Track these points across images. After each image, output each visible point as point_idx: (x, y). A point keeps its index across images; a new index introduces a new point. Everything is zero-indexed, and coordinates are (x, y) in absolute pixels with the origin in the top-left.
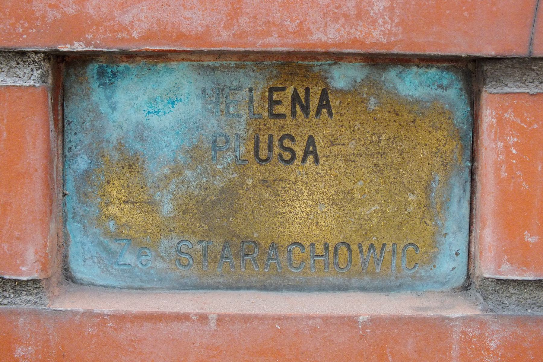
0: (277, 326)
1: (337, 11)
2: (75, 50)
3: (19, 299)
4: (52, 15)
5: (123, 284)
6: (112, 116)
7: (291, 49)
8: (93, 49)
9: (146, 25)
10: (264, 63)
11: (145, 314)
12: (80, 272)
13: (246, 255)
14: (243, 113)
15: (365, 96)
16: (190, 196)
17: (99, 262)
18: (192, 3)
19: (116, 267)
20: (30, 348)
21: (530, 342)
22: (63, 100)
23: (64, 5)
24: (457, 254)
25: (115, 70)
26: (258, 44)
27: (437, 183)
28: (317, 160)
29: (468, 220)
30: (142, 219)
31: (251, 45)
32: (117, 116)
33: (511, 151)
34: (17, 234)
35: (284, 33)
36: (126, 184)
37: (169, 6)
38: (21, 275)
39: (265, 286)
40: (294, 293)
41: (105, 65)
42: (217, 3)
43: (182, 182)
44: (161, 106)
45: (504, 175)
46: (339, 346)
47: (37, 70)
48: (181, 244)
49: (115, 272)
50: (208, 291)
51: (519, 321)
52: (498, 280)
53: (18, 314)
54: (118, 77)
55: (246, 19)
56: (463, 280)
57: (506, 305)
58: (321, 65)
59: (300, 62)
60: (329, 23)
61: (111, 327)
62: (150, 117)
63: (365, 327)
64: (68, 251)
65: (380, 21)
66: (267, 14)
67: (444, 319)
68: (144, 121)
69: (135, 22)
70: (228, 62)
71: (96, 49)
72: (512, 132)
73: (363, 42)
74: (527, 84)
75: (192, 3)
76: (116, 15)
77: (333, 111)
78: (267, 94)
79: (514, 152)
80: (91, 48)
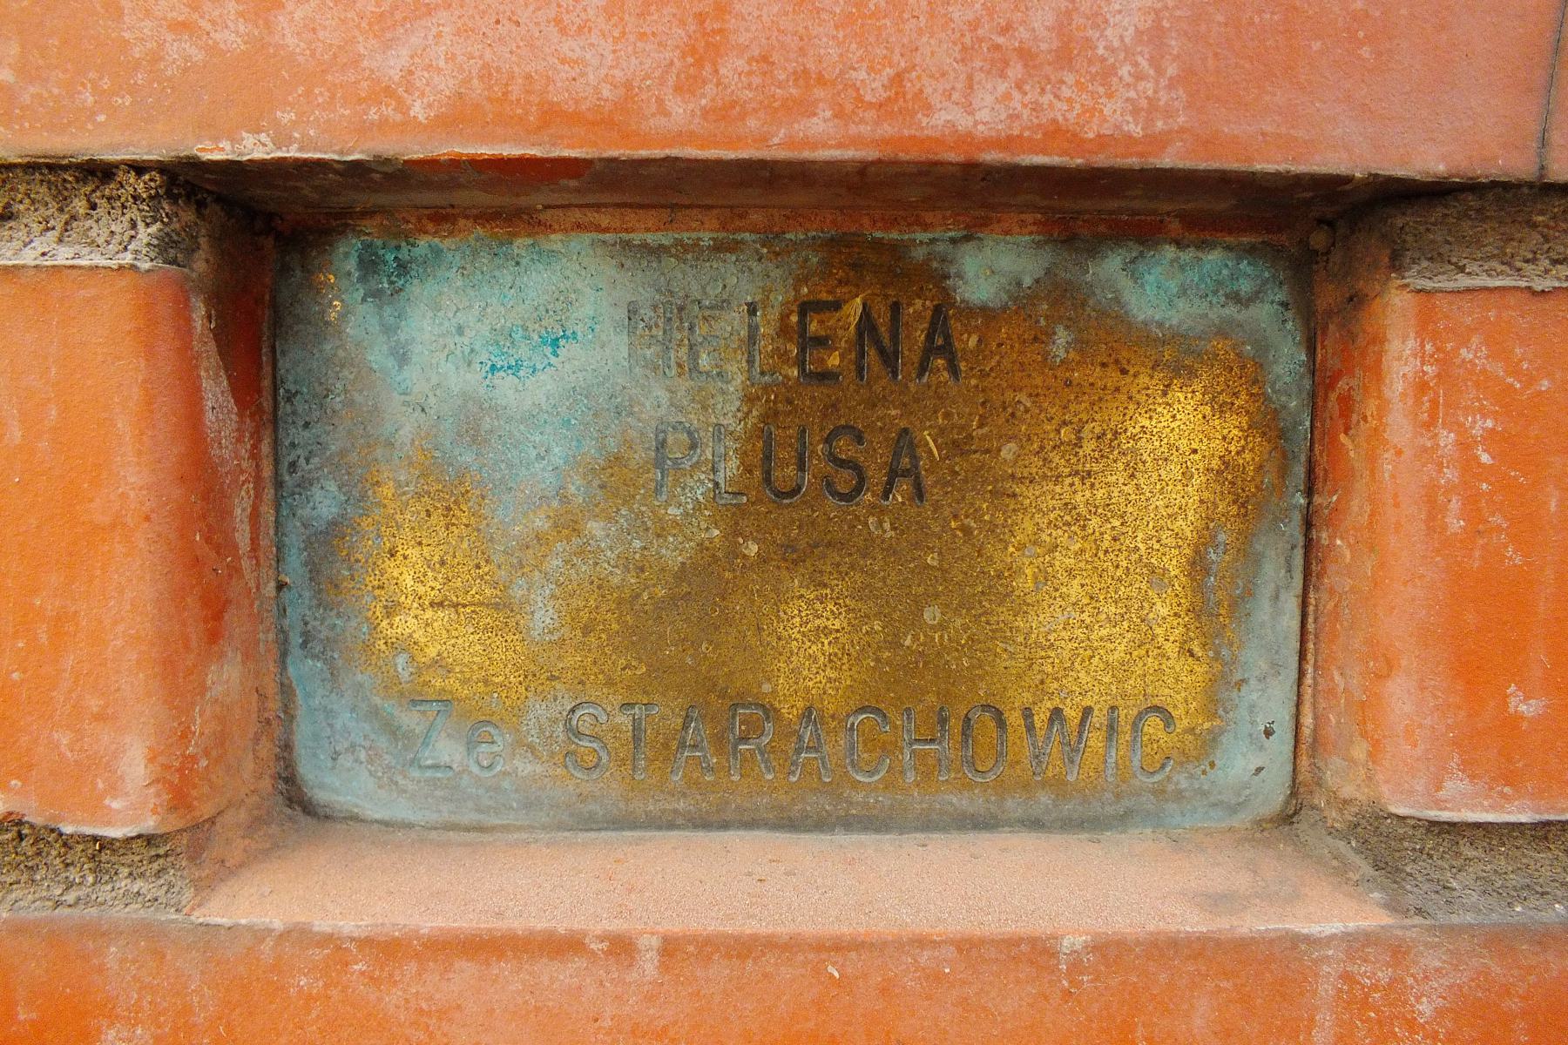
0: (831, 969)
1: (1000, 40)
2: (245, 158)
3: (109, 887)
4: (179, 50)
5: (433, 817)
6: (398, 379)
7: (871, 154)
8: (298, 155)
9: (451, 82)
10: (788, 236)
11: (457, 937)
12: (322, 786)
13: (744, 739)
14: (735, 369)
15: (1043, 322)
16: (599, 587)
17: (370, 761)
18: (583, 16)
19: (416, 774)
20: (139, 1032)
21: (1523, 998)
22: (275, 336)
23: (214, 23)
24: (1268, 733)
25: (404, 254)
26: (776, 140)
27: (1220, 551)
28: (919, 493)
29: (1295, 644)
30: (478, 647)
31: (755, 141)
32: (411, 375)
33: (1477, 458)
34: (94, 703)
35: (849, 107)
36: (436, 558)
37: (518, 24)
38: (109, 824)
39: (790, 818)
40: (863, 837)
41: (379, 243)
42: (655, 17)
43: (580, 552)
44: (523, 351)
45: (1456, 524)
46: (1004, 1022)
47: (148, 225)
48: (579, 713)
49: (411, 787)
50: (649, 834)
51: (1499, 940)
52: (1433, 823)
53: (101, 933)
54: (413, 273)
55: (741, 63)
56: (1281, 798)
57: (1455, 894)
58: (933, 241)
59: (878, 234)
60: (978, 76)
61: (363, 973)
62: (496, 381)
63: (1076, 967)
64: (291, 732)
65: (1125, 71)
66: (801, 49)
67: (1295, 941)
68: (482, 391)
69: (418, 73)
70: (694, 235)
71: (306, 156)
72: (1479, 400)
73: (1075, 135)
74: (1519, 264)
75: (583, 16)
76: (362, 51)
77: (963, 366)
78: (794, 319)
79: (1485, 458)
80: (293, 152)
